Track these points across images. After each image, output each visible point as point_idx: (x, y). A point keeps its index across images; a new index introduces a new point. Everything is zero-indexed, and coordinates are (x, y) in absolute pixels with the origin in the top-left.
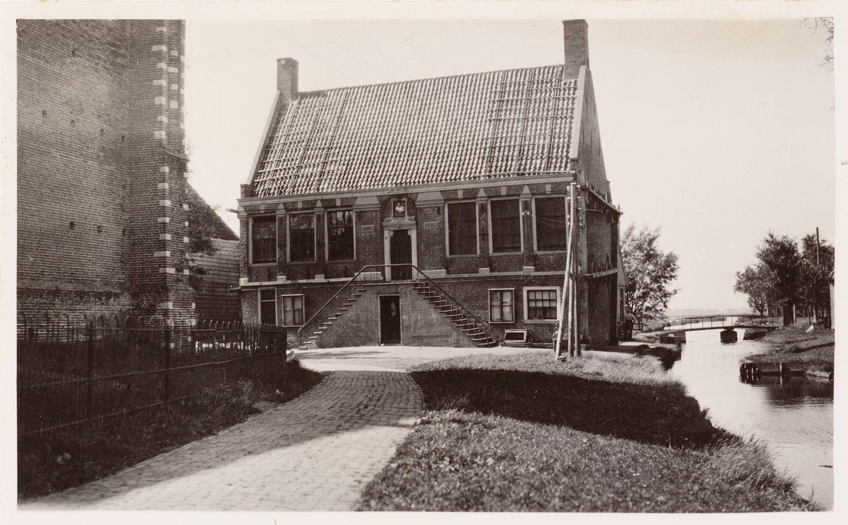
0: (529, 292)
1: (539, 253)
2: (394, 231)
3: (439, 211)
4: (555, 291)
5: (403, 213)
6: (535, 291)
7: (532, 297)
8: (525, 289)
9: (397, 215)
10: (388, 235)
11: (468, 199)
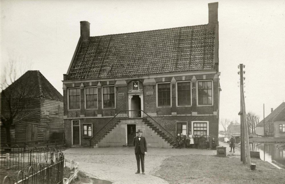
0: (194, 123)
1: (191, 105)
2: (133, 96)
3: (154, 86)
4: (206, 123)
5: (137, 88)
6: (197, 123)
7: (195, 125)
8: (192, 122)
9: (134, 88)
10: (130, 97)
11: (207, 79)
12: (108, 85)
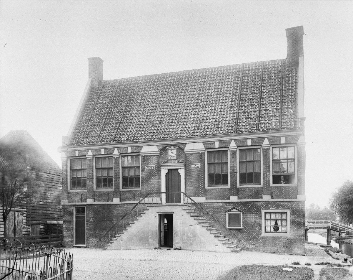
0: (266, 213)
4: (286, 213)
6: (270, 213)
10: (164, 172)
11: (253, 146)
12: (77, 157)
